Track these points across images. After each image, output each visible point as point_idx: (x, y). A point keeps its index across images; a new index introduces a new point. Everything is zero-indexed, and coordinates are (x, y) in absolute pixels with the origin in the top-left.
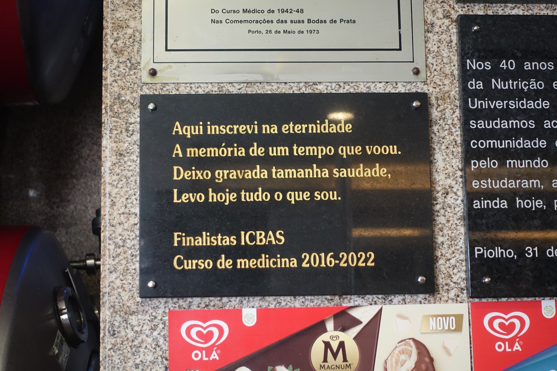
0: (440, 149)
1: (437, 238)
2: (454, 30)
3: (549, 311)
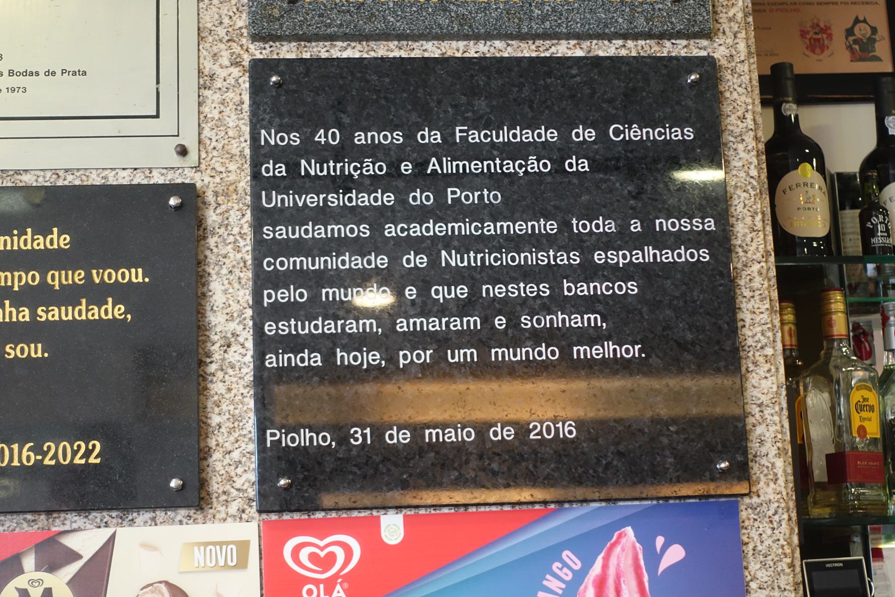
0: (218, 274)
1: (210, 418)
2: (245, 84)
3: (392, 532)
